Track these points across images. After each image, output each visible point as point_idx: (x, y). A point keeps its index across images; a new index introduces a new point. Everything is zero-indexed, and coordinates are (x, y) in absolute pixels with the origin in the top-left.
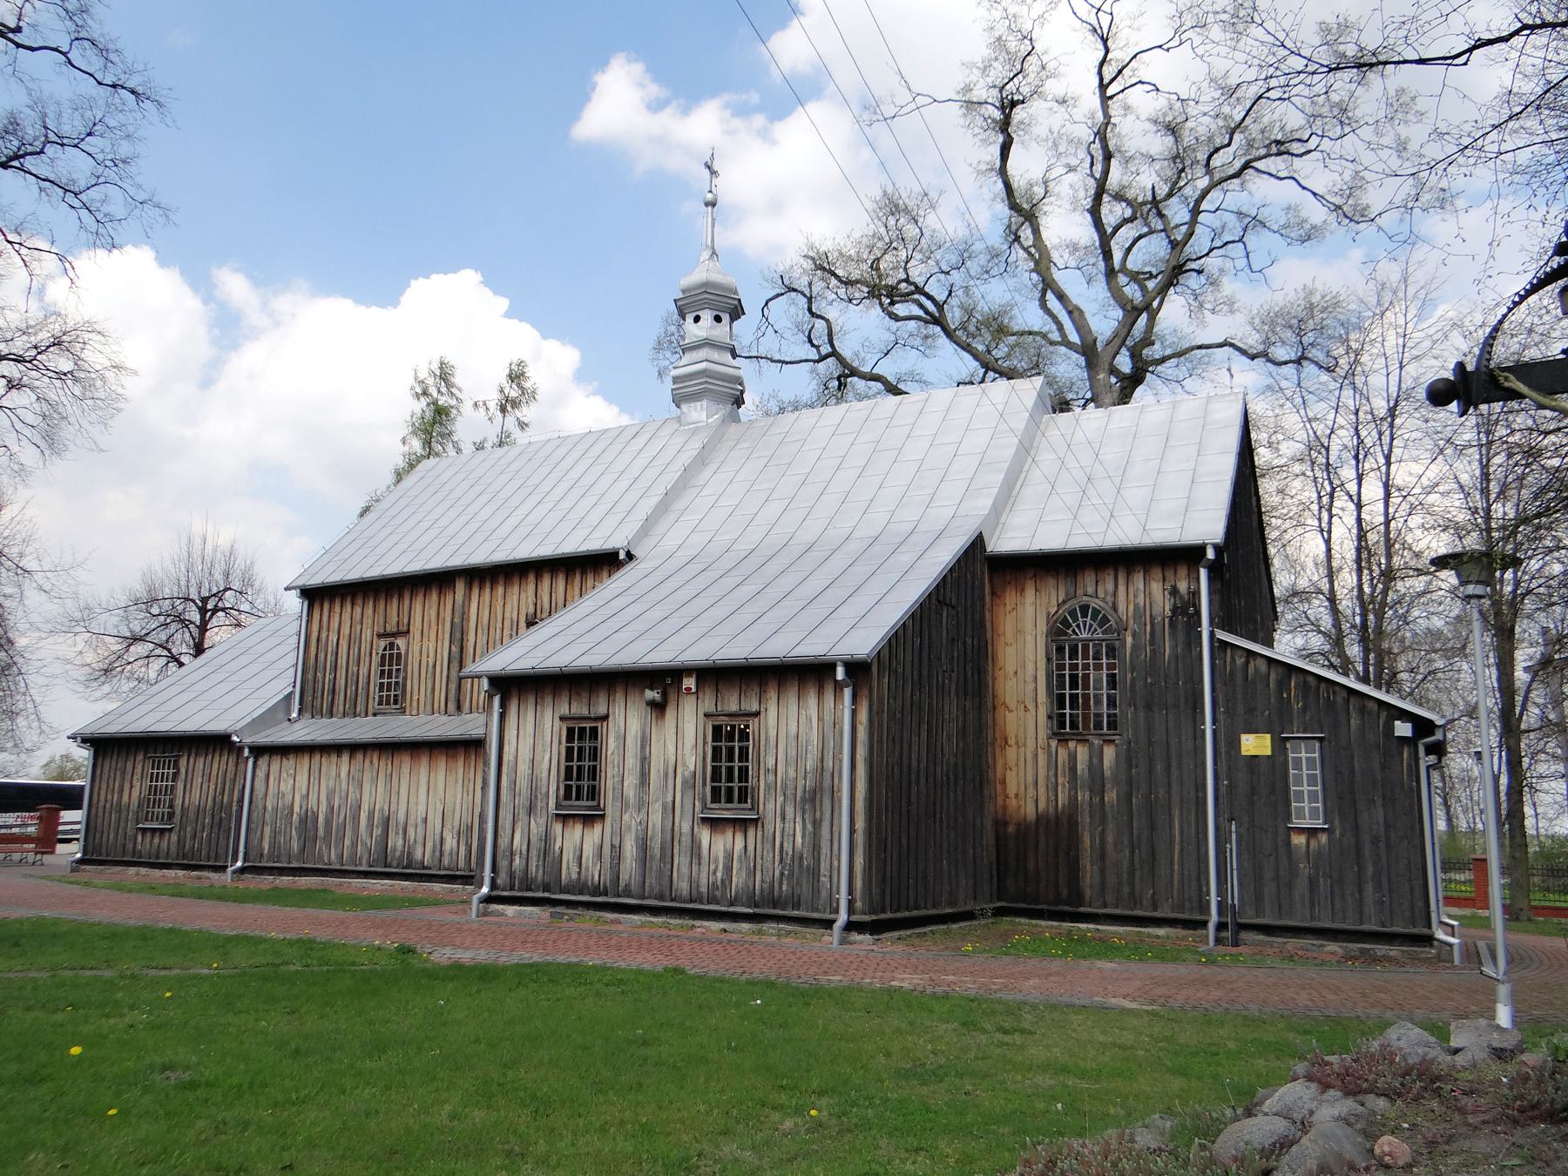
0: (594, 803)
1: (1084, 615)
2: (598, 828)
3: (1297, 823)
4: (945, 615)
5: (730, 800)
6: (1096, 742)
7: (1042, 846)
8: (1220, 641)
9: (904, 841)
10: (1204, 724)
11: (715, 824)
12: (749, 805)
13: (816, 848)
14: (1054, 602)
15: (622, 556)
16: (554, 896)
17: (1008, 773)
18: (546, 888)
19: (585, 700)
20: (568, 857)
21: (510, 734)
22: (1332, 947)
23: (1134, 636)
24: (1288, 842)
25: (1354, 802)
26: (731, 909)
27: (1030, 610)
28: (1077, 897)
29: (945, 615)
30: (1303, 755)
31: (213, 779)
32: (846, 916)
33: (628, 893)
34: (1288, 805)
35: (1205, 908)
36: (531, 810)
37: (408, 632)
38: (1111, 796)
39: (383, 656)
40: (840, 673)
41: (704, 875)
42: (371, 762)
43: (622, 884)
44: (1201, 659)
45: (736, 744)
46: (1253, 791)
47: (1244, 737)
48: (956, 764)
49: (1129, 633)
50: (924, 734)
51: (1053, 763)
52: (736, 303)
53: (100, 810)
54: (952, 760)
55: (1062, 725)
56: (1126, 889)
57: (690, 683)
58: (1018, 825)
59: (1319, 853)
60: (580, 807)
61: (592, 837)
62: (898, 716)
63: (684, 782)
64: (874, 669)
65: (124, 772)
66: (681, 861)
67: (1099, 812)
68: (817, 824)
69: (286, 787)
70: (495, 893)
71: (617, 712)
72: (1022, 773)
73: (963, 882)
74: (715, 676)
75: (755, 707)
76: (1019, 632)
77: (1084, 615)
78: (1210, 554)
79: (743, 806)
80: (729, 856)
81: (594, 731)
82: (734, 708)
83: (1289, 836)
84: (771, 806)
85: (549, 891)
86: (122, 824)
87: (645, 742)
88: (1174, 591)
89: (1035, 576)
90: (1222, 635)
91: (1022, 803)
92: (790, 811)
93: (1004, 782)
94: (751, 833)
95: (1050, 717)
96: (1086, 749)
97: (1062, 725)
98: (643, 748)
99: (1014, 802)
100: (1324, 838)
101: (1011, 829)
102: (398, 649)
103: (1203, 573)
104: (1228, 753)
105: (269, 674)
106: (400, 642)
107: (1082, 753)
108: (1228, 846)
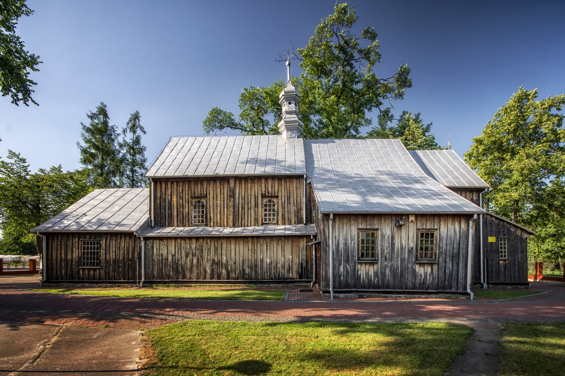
0: (374, 259)
11: (421, 264)
16: (359, 290)
18: (355, 287)
22: (509, 287)
33: (388, 287)
37: (206, 197)
42: (207, 243)
47: (489, 237)
57: (412, 218)
60: (368, 260)
61: (371, 270)
65: (66, 247)
69: (164, 252)
74: (421, 216)
85: (356, 288)
87: (393, 238)
100: (507, 262)
102: (203, 203)
106: (204, 201)
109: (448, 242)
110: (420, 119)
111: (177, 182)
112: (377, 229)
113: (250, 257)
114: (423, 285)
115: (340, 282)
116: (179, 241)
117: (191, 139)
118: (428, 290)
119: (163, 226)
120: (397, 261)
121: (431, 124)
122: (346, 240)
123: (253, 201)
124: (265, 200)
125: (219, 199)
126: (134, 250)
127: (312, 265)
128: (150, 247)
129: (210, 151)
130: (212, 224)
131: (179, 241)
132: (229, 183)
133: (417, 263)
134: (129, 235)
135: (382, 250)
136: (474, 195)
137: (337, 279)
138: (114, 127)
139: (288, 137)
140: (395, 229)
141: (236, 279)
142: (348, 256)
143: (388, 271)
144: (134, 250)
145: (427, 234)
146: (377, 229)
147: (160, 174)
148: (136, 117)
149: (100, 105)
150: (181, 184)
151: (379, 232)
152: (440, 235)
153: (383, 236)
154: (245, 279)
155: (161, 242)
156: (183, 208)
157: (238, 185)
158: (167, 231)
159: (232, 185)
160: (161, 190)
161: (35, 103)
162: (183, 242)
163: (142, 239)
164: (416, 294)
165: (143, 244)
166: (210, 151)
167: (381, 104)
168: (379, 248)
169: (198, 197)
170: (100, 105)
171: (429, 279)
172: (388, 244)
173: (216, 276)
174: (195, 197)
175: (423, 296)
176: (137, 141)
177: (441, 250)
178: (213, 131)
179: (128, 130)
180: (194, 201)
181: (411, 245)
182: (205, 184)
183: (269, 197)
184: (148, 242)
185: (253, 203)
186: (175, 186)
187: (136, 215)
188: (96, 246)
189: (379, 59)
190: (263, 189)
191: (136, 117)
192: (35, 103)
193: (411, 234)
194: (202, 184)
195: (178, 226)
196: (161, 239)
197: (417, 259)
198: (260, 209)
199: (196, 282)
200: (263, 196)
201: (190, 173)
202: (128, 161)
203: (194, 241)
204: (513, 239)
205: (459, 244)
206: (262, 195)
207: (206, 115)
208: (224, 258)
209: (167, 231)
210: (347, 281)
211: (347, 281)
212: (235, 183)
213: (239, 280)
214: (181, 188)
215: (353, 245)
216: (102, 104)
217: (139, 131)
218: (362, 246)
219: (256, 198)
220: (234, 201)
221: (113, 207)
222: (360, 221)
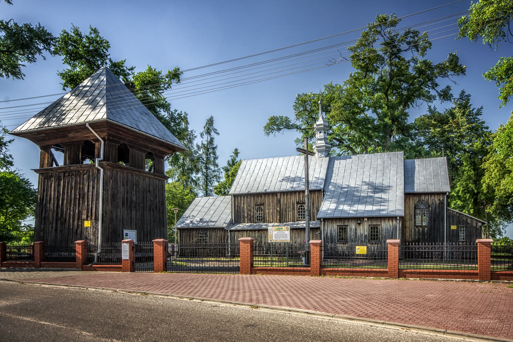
1: (422, 204)
3: (460, 240)
19: (343, 222)
21: (326, 228)
33: (340, 256)
34: (459, 237)
40: (398, 218)
42: (264, 233)
51: (415, 230)
63: (365, 236)
65: (190, 236)
74: (370, 218)
77: (422, 204)
78: (447, 194)
81: (345, 229)
82: (375, 224)
87: (356, 230)
88: (439, 200)
106: (262, 207)
109: (386, 231)
110: (470, 104)
111: (247, 196)
112: (347, 225)
115: (328, 254)
116: (249, 232)
117: (254, 161)
119: (239, 223)
120: (359, 242)
121: (482, 108)
122: (331, 231)
123: (291, 206)
124: (299, 205)
125: (271, 205)
126: (224, 237)
128: (233, 236)
129: (267, 171)
131: (249, 232)
132: (277, 196)
134: (222, 229)
135: (351, 236)
136: (441, 196)
138: (193, 131)
139: (319, 157)
140: (357, 225)
142: (332, 239)
144: (224, 237)
146: (347, 225)
147: (237, 192)
148: (210, 122)
150: (249, 197)
151: (349, 227)
152: (382, 228)
153: (351, 229)
157: (282, 197)
158: (240, 226)
159: (279, 197)
160: (238, 201)
162: (251, 233)
163: (229, 231)
165: (229, 234)
166: (267, 171)
167: (437, 85)
168: (349, 235)
169: (259, 205)
174: (258, 205)
176: (211, 141)
178: (272, 133)
179: (204, 134)
180: (257, 207)
181: (366, 234)
182: (263, 197)
183: (301, 203)
184: (232, 233)
185: (291, 207)
186: (246, 199)
187: (224, 216)
189: (430, 46)
190: (298, 199)
191: (210, 122)
193: (366, 228)
194: (261, 197)
195: (248, 223)
196: (239, 231)
197: (369, 241)
198: (296, 211)
200: (298, 203)
201: (253, 191)
202: (203, 159)
203: (257, 232)
204: (469, 227)
205: (392, 233)
206: (297, 202)
207: (266, 121)
209: (240, 226)
210: (331, 252)
211: (331, 252)
212: (281, 196)
214: (249, 200)
217: (213, 133)
219: (293, 204)
220: (280, 207)
221: (210, 212)
222: (338, 221)
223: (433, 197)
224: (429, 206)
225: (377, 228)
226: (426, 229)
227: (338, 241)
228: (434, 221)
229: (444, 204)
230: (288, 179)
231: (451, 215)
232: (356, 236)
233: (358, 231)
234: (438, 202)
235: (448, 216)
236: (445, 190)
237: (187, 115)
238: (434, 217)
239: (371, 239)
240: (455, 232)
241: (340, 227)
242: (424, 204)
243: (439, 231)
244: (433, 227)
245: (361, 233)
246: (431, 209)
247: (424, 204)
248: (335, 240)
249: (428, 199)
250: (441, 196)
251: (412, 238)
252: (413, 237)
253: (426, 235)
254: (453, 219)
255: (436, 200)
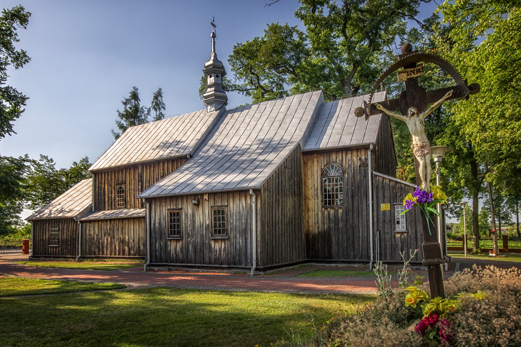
0: (179, 236)
1: (332, 169)
2: (181, 243)
4: (287, 171)
5: (220, 233)
6: (336, 208)
7: (320, 241)
8: (374, 175)
9: (274, 243)
10: (369, 201)
11: (216, 240)
12: (225, 235)
13: (246, 246)
14: (323, 165)
15: (188, 156)
17: (310, 219)
18: (166, 262)
20: (173, 252)
23: (99, 283)
24: (395, 237)
25: (416, 223)
26: (221, 266)
27: (316, 168)
28: (331, 257)
29: (287, 171)
30: (400, 209)
31: (70, 231)
32: (255, 266)
35: (369, 258)
36: (161, 238)
37: (125, 183)
38: (341, 225)
39: (118, 191)
41: (213, 256)
43: (189, 259)
44: (368, 181)
45: (221, 216)
46: (384, 221)
48: (292, 218)
49: (346, 174)
50: (280, 209)
51: (323, 214)
52: (223, 70)
53: (37, 242)
54: (291, 217)
55: (326, 204)
56: (345, 253)
58: (313, 235)
59: (404, 239)
62: (271, 204)
63: (206, 227)
64: (262, 191)
66: (206, 252)
67: (337, 229)
68: (246, 239)
70: (151, 264)
71: (185, 206)
72: (314, 219)
73: (295, 254)
74: (214, 194)
75: (226, 204)
76: (312, 175)
77: (332, 169)
78: (371, 147)
79: (223, 235)
80: (220, 249)
82: (220, 205)
83: (395, 235)
84: (232, 234)
85: (167, 262)
86: (44, 245)
87: (193, 216)
88: (360, 159)
89: (317, 157)
90: (374, 173)
91: (314, 228)
92: (238, 235)
93: (308, 222)
94: (227, 242)
95: (322, 201)
96: (333, 211)
97: (326, 204)
98: (193, 218)
99: (312, 228)
100: (406, 235)
101: (311, 236)
103: (369, 153)
104: (377, 210)
105: (85, 197)
107: (332, 211)
108: (376, 239)
112: (181, 209)
113: (143, 235)
114: (217, 261)
118: (222, 265)
127: (368, 243)
130: (129, 206)
133: (213, 239)
137: (154, 254)
138: (144, 108)
141: (134, 255)
143: (190, 247)
145: (330, 204)
148: (158, 95)
149: (133, 89)
153: (186, 215)
154: (141, 255)
155: (91, 225)
156: (111, 194)
158: (99, 215)
161: (15, 133)
164: (212, 269)
168: (184, 225)
170: (133, 89)
171: (223, 254)
172: (190, 222)
173: (121, 253)
174: (118, 184)
175: (217, 271)
177: (232, 226)
188: (221, 222)
191: (158, 95)
192: (15, 133)
196: (94, 221)
199: (110, 258)
208: (127, 237)
213: (136, 256)
215: (165, 223)
216: (134, 88)
218: (214, 223)
223: (349, 156)
224: (344, 173)
225: (223, 212)
226: (340, 211)
227: (169, 237)
228: (352, 197)
229: (367, 166)
230: (165, 145)
231: (380, 186)
232: (194, 226)
233: (197, 218)
234: (357, 163)
235: (375, 187)
236: (366, 141)
237: (137, 89)
238: (352, 190)
239: (215, 230)
240: (388, 214)
241: (171, 211)
242: (336, 168)
243: (362, 215)
244: (351, 209)
245: (200, 222)
246: (347, 176)
247: (336, 168)
248: (165, 234)
249: (342, 159)
250: (363, 153)
251: (318, 227)
252: (320, 226)
253: (340, 222)
254: (384, 192)
255: (354, 159)
